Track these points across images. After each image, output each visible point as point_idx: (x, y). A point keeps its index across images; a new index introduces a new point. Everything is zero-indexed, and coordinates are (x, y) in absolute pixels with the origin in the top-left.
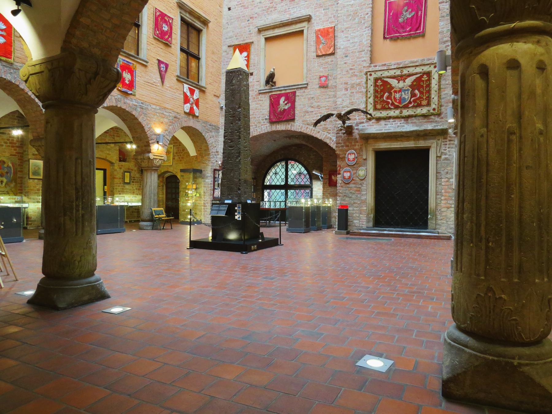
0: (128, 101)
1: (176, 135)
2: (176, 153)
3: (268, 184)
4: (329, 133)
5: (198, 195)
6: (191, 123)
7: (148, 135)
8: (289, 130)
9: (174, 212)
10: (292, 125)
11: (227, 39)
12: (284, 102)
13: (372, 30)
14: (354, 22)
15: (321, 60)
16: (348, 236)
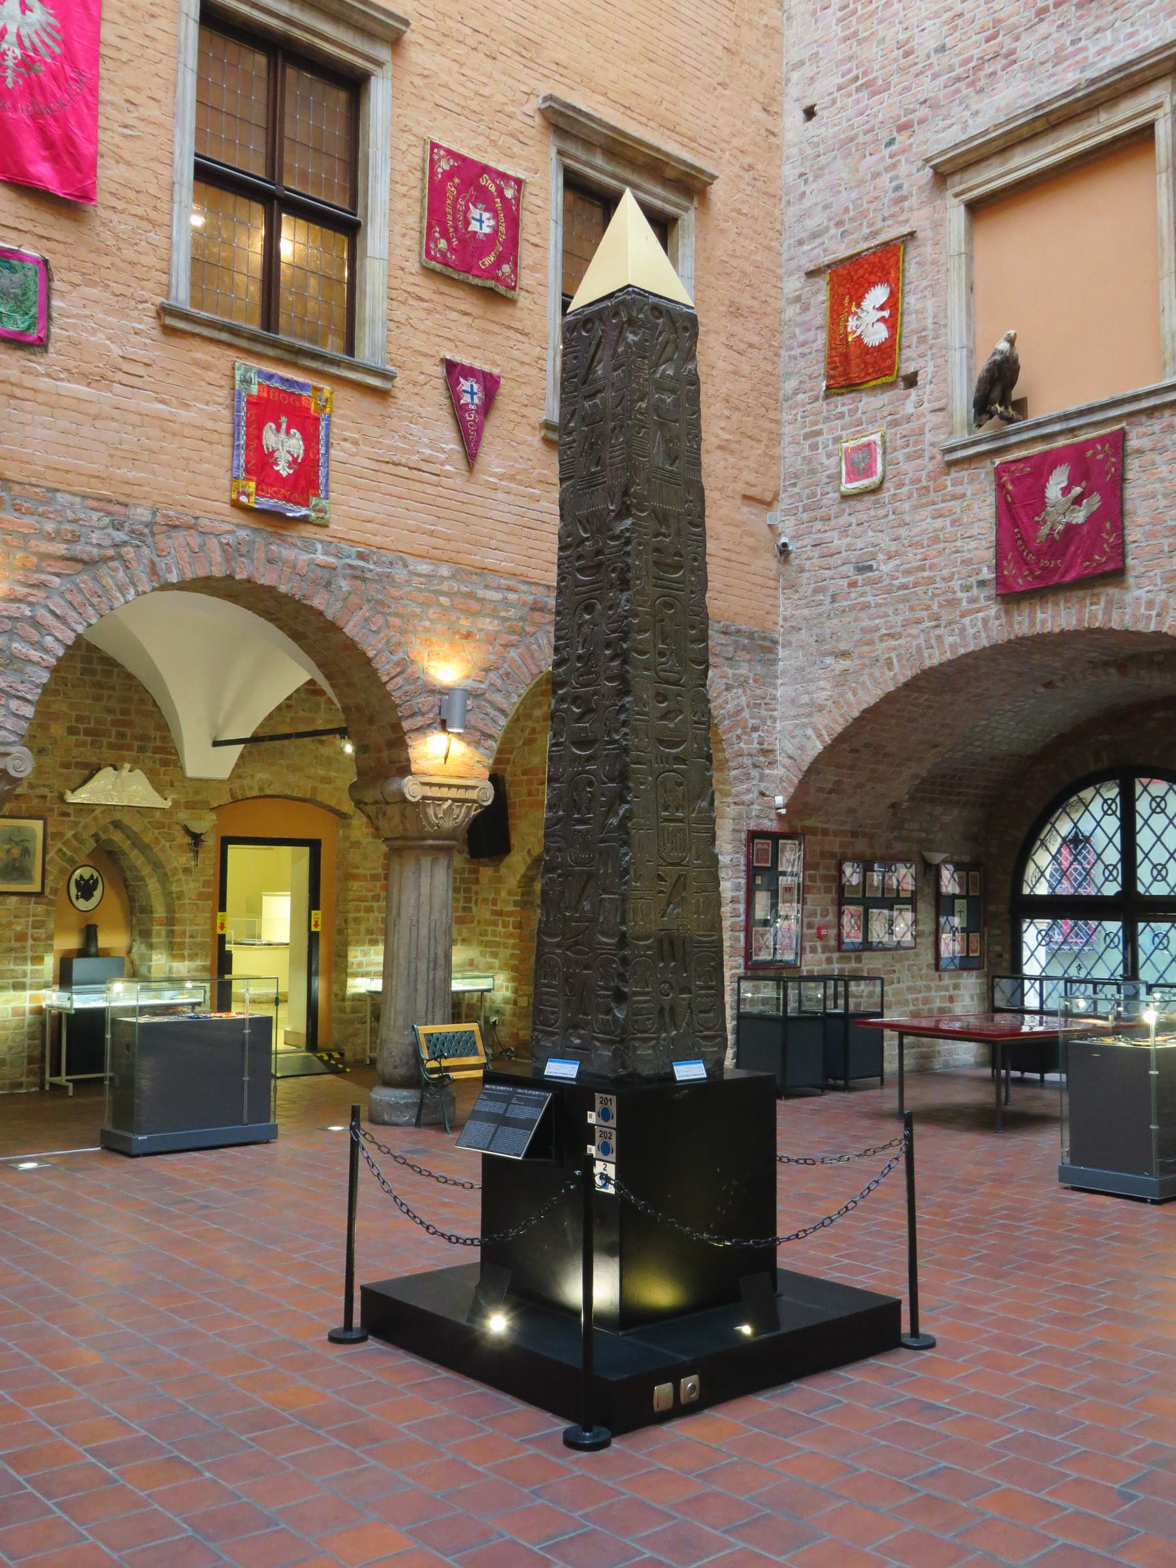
0: (287, 553)
7: (397, 697)
8: (1099, 630)
10: (1110, 602)
11: (801, 243)
12: (1066, 491)
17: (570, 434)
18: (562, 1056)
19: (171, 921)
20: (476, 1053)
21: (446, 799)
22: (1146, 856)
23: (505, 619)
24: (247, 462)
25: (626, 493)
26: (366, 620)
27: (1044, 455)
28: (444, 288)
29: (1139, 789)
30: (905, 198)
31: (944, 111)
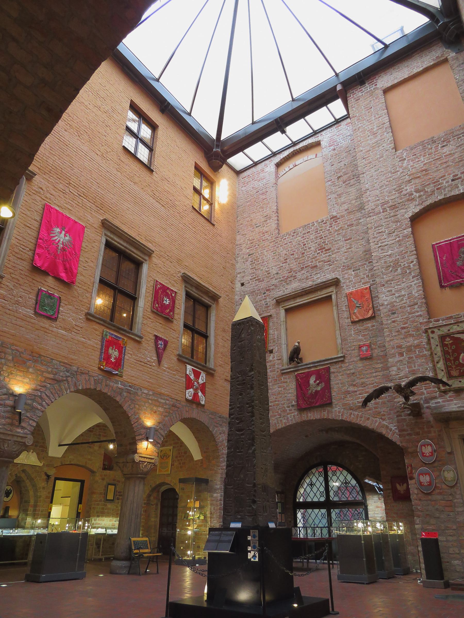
0: (111, 384)
1: (173, 429)
2: (176, 457)
3: (301, 500)
4: (384, 420)
5: (202, 517)
6: (195, 413)
8: (326, 419)
9: (167, 546)
10: (328, 412)
12: (315, 382)
13: (422, 279)
14: (396, 273)
15: (358, 327)
16: (449, 590)
17: (234, 351)
18: (235, 521)
19: (35, 506)
20: (148, 548)
21: (145, 462)
22: (332, 489)
23: (165, 408)
24: (104, 357)
25: (252, 366)
26: (130, 405)
27: (308, 372)
28: (156, 317)
30: (268, 307)
31: (278, 287)
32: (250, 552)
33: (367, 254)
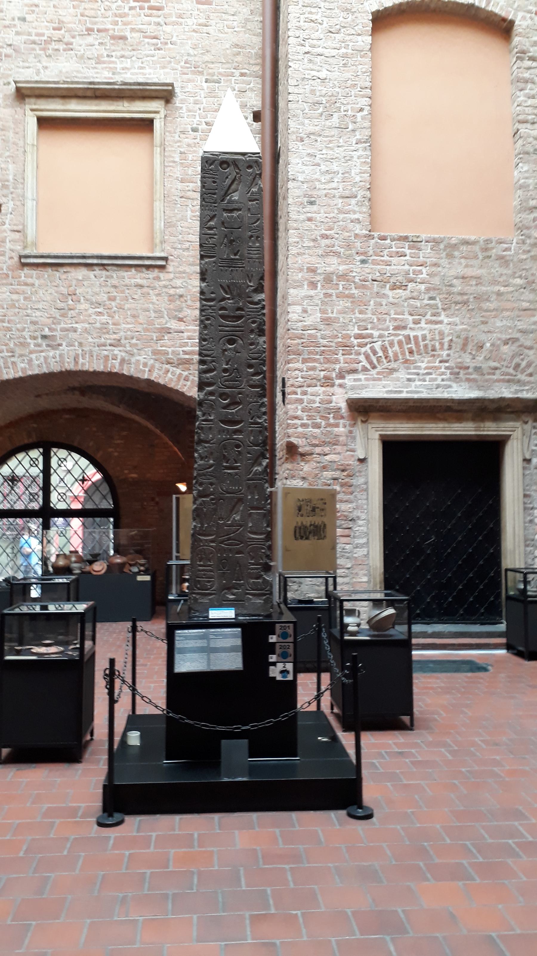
14: (328, 123)
17: (210, 228)
18: (220, 605)
29: (52, 454)
32: (274, 664)
33: (238, 54)
